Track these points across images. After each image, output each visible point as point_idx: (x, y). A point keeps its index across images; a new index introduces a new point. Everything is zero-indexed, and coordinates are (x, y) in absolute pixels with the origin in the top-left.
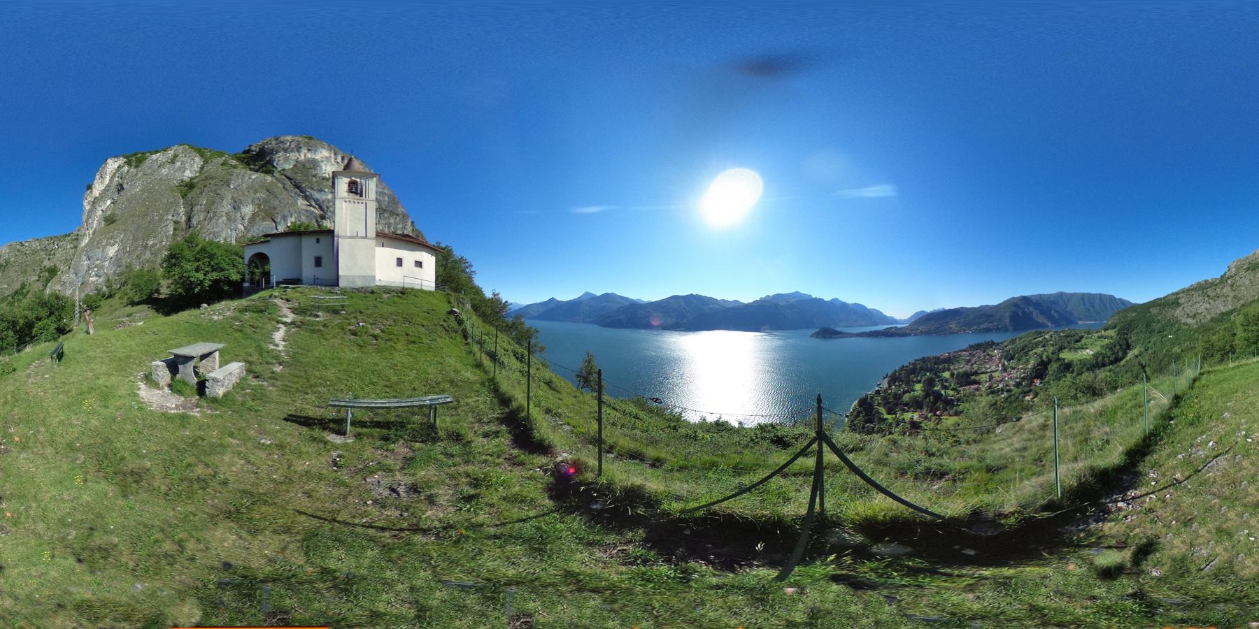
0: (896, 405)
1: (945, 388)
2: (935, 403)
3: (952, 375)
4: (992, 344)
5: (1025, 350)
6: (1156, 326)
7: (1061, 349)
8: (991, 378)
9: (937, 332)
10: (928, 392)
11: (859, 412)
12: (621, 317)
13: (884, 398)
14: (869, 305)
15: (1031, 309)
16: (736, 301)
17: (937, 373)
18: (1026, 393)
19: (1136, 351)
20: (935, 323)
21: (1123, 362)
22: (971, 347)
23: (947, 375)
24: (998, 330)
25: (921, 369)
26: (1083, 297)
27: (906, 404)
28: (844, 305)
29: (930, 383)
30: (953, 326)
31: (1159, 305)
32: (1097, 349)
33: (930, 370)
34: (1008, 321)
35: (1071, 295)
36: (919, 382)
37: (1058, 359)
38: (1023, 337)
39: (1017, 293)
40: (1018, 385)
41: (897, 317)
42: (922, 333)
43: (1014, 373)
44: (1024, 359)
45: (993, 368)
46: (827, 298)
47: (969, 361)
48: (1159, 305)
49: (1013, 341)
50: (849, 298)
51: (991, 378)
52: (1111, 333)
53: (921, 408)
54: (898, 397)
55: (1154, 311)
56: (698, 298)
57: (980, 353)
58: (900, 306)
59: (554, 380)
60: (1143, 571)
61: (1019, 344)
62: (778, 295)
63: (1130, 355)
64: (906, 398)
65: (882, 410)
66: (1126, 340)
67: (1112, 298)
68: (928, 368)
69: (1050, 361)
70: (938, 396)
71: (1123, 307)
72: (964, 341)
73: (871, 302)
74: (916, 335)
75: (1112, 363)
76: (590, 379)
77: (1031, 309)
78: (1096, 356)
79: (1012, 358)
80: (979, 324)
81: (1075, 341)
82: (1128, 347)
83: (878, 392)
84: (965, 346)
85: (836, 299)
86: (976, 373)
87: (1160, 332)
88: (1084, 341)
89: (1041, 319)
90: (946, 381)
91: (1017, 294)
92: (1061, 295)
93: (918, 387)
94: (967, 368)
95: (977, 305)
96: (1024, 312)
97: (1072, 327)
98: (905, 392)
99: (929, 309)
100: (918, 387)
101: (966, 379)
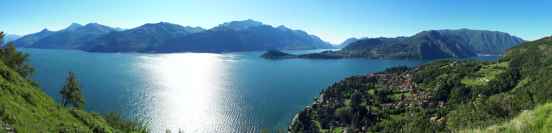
0: (330, 119)
1: (370, 104)
2: (361, 118)
3: (376, 92)
4: (404, 69)
5: (432, 75)
6: (544, 61)
7: (462, 76)
8: (403, 97)
9: (365, 55)
10: (356, 107)
11: (299, 126)
12: (103, 43)
13: (320, 113)
14: (310, 32)
15: (439, 41)
16: (199, 28)
17: (363, 90)
18: (431, 114)
19: (525, 81)
20: (361, 48)
21: (514, 90)
22: (388, 70)
23: (371, 92)
24: (410, 57)
25: (351, 86)
26: (486, 36)
27: (338, 119)
28: (289, 31)
29: (357, 99)
30: (374, 52)
31: (547, 43)
32: (492, 78)
33: (358, 88)
34: (419, 50)
35: (473, 32)
36: (348, 98)
37: (460, 85)
38: (431, 64)
39: (428, 28)
40: (425, 106)
41: (332, 43)
42: (352, 56)
43: (422, 95)
44: (431, 83)
45: (405, 90)
46: (275, 25)
47: (386, 82)
48: (547, 43)
49: (423, 67)
50: (293, 26)
51: (403, 97)
52: (505, 64)
53: (350, 123)
54: (331, 111)
55: (542, 48)
56: (168, 25)
57: (395, 76)
58: (335, 33)
59: (32, 94)
60: (6, 50)
61: (427, 70)
62: (234, 23)
63: (520, 85)
64: (338, 112)
65: (318, 124)
66: (518, 71)
67: (507, 35)
68: (355, 86)
69: (453, 86)
70: (364, 111)
71: (515, 43)
72: (387, 64)
73: (312, 29)
74: (347, 57)
75: (504, 90)
76: (69, 95)
77: (439, 41)
78: (491, 83)
79: (421, 81)
80: (395, 52)
81: (474, 70)
82: (519, 77)
83: (315, 106)
84: (384, 69)
85: (283, 26)
86: (391, 93)
87: (546, 65)
88: (481, 70)
89: (447, 50)
90: (371, 97)
91: (428, 29)
92: (464, 31)
93: (348, 102)
94: (384, 88)
95: (394, 36)
96: (433, 44)
97: (472, 58)
98: (336, 107)
99: (359, 37)
100: (348, 102)
101: (384, 97)
